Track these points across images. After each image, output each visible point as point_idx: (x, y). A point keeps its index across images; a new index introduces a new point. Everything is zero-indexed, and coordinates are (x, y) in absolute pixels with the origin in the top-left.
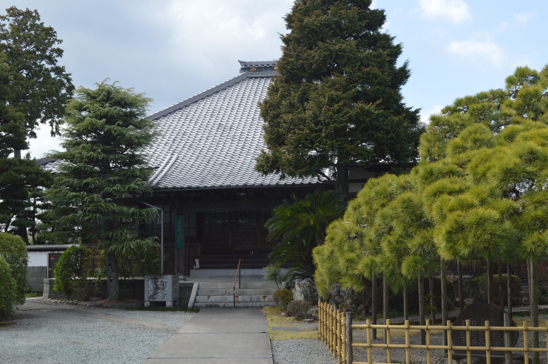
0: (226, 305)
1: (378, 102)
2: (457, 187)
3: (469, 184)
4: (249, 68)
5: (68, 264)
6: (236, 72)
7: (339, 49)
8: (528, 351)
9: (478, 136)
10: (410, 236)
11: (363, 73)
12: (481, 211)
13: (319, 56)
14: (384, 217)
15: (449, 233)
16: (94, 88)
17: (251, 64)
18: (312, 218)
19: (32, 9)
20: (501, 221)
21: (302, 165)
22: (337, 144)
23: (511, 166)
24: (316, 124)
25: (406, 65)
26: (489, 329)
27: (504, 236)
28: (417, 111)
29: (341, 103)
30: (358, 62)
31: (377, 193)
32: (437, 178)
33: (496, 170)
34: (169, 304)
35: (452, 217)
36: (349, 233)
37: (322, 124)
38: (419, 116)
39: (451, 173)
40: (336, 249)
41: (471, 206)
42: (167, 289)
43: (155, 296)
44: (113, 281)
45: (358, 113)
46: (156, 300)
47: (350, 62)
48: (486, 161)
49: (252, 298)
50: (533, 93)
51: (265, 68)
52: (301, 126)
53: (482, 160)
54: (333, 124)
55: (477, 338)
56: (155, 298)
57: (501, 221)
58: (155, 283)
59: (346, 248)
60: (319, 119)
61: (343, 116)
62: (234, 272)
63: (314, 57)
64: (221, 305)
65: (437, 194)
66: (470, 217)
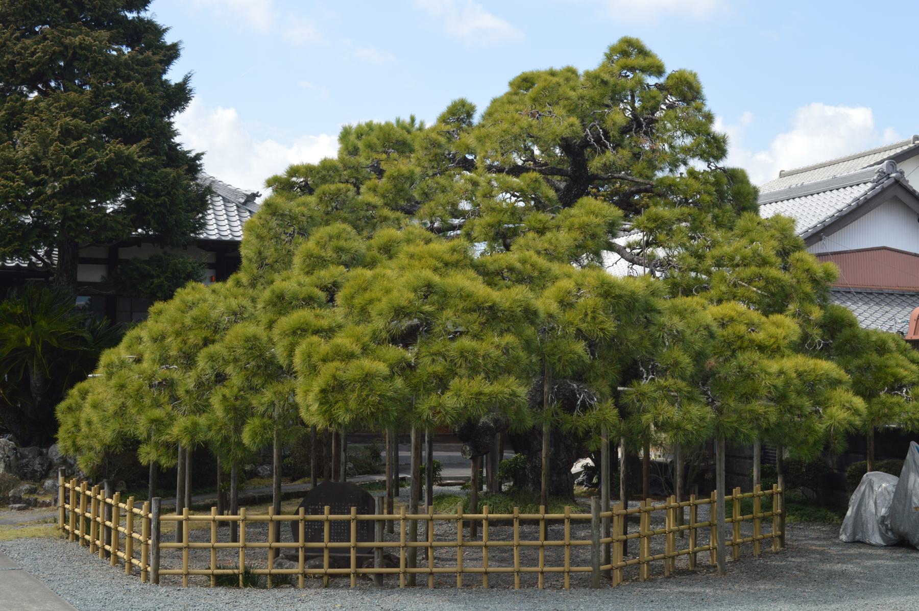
1: (144, 142)
2: (325, 323)
3: (340, 319)
7: (81, 44)
8: (405, 546)
9: (342, 243)
11: (120, 91)
12: (367, 364)
13: (45, 52)
14: (212, 358)
15: (323, 391)
18: (28, 334)
20: (390, 377)
21: (7, 240)
22: (72, 208)
23: (404, 303)
24: (37, 171)
25: (186, 79)
26: (355, 519)
27: (394, 398)
28: (198, 157)
29: (83, 141)
30: (111, 70)
31: (195, 319)
33: (383, 305)
35: (328, 370)
37: (46, 173)
38: (201, 165)
39: (309, 301)
40: (129, 403)
41: (351, 356)
45: (111, 159)
47: (98, 69)
48: (365, 290)
50: (407, 175)
52: (10, 174)
53: (360, 288)
54: (68, 174)
55: (340, 531)
57: (390, 377)
59: (148, 401)
60: (44, 163)
61: (86, 163)
63: (33, 54)
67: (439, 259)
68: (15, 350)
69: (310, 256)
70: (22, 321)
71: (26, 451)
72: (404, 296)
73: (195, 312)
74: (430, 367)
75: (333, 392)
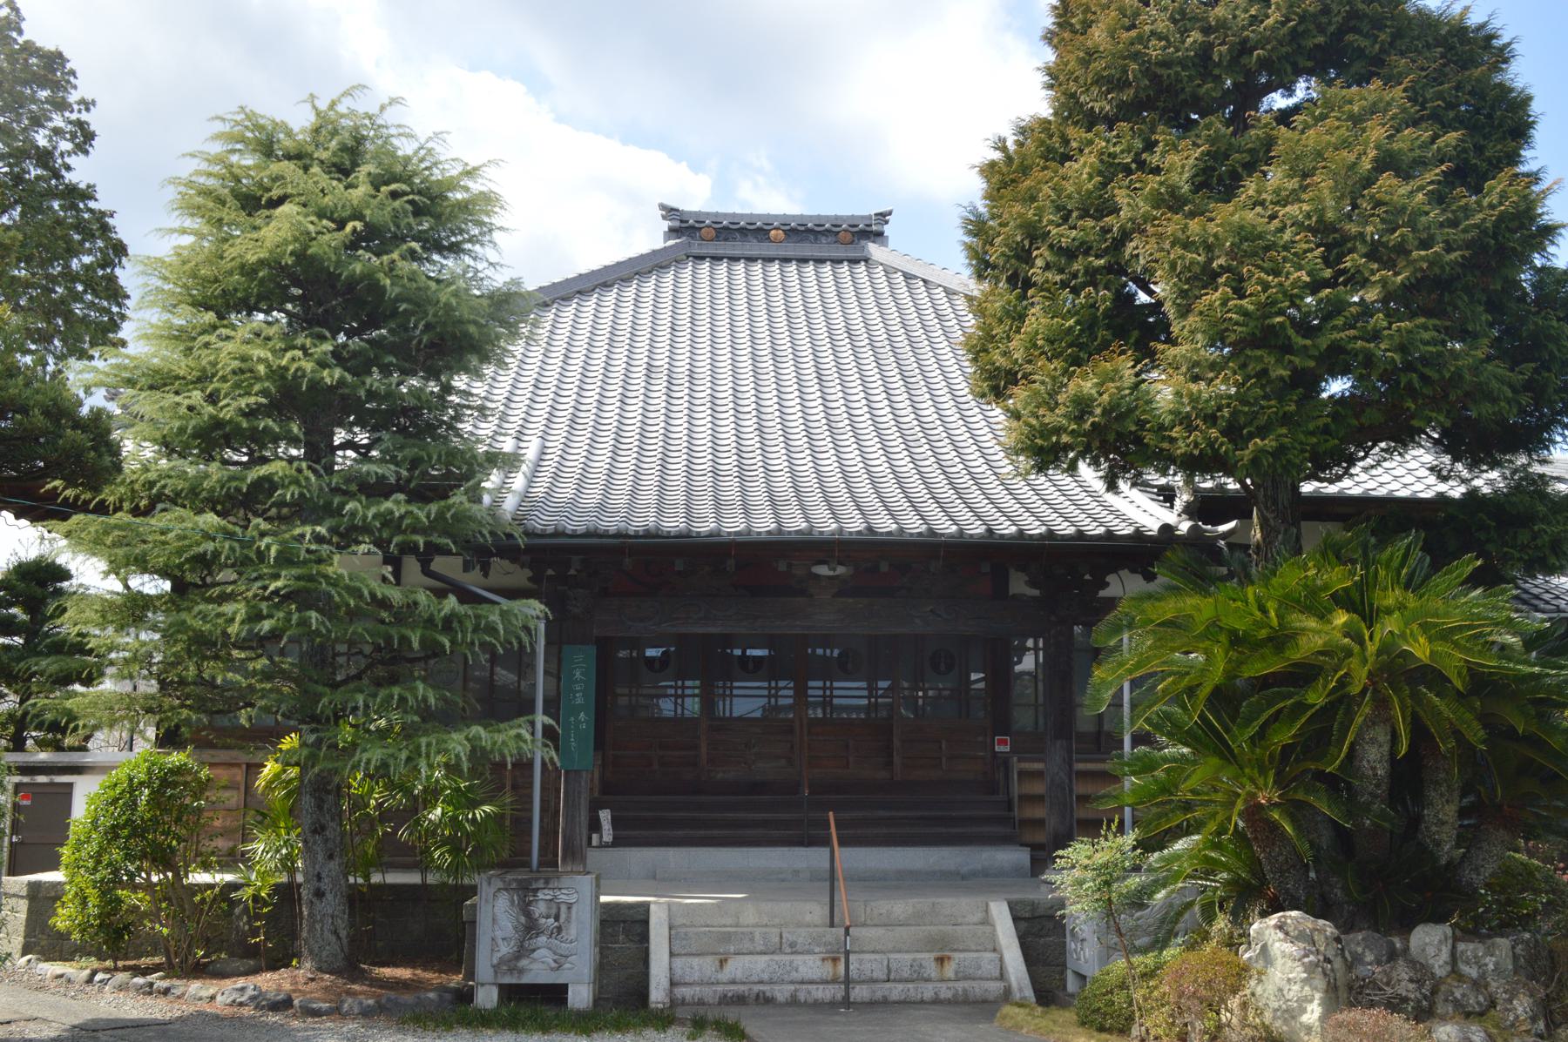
0: (802, 997)
4: (692, 227)
5: (129, 822)
6: (651, 237)
16: (300, 120)
17: (699, 217)
34: (580, 996)
42: (572, 931)
43: (524, 963)
44: (329, 897)
46: (526, 979)
49: (894, 966)
51: (743, 231)
56: (521, 971)
58: (525, 909)
62: (815, 858)
64: (781, 993)
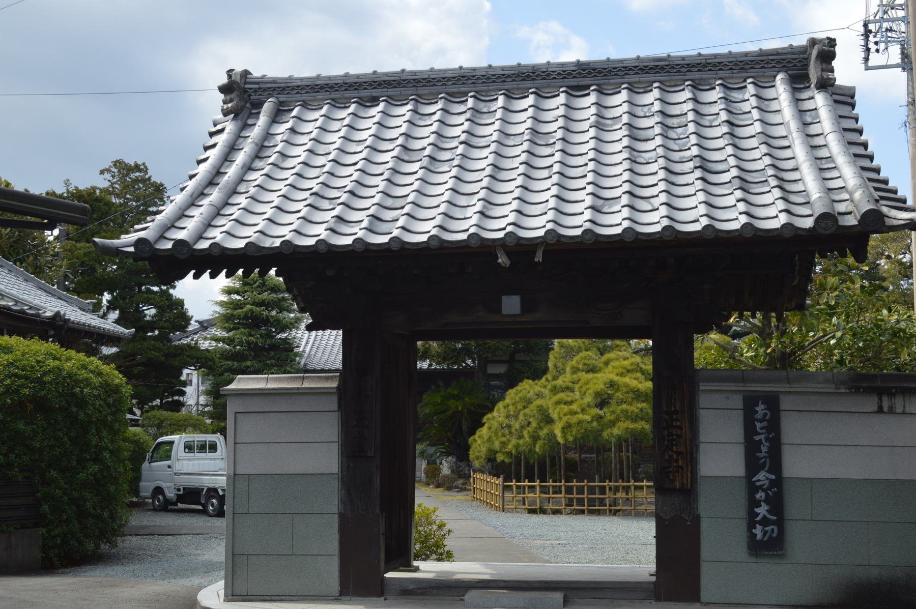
2: (569, 399)
9: (586, 361)
10: (541, 428)
12: (581, 416)
14: (525, 415)
15: (563, 428)
19: (140, 163)
32: (559, 392)
35: (565, 419)
36: (501, 424)
41: (576, 413)
65: (558, 403)
66: (574, 419)
67: (624, 368)
68: (454, 413)
69: (573, 368)
70: (457, 398)
71: (461, 464)
72: (601, 386)
73: (521, 395)
74: (609, 417)
75: (567, 428)
